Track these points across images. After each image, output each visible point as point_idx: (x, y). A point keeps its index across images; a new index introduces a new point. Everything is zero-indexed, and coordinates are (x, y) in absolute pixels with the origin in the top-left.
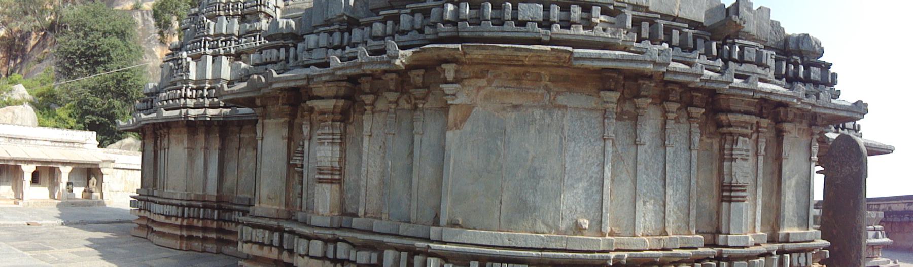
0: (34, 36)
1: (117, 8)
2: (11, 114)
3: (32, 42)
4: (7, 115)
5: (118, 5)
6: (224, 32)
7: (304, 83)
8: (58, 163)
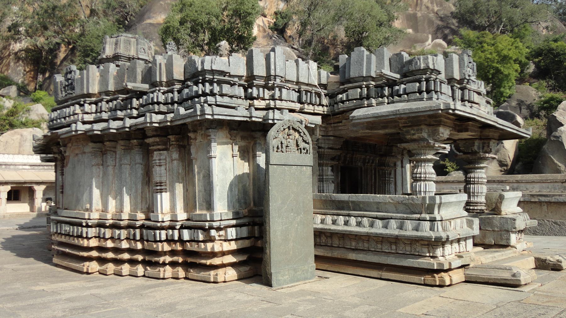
0: (63, 48)
1: (149, 21)
2: (19, 137)
3: (62, 55)
4: (15, 138)
5: (149, 18)
6: (373, 74)
7: (313, 126)
8: (31, 183)
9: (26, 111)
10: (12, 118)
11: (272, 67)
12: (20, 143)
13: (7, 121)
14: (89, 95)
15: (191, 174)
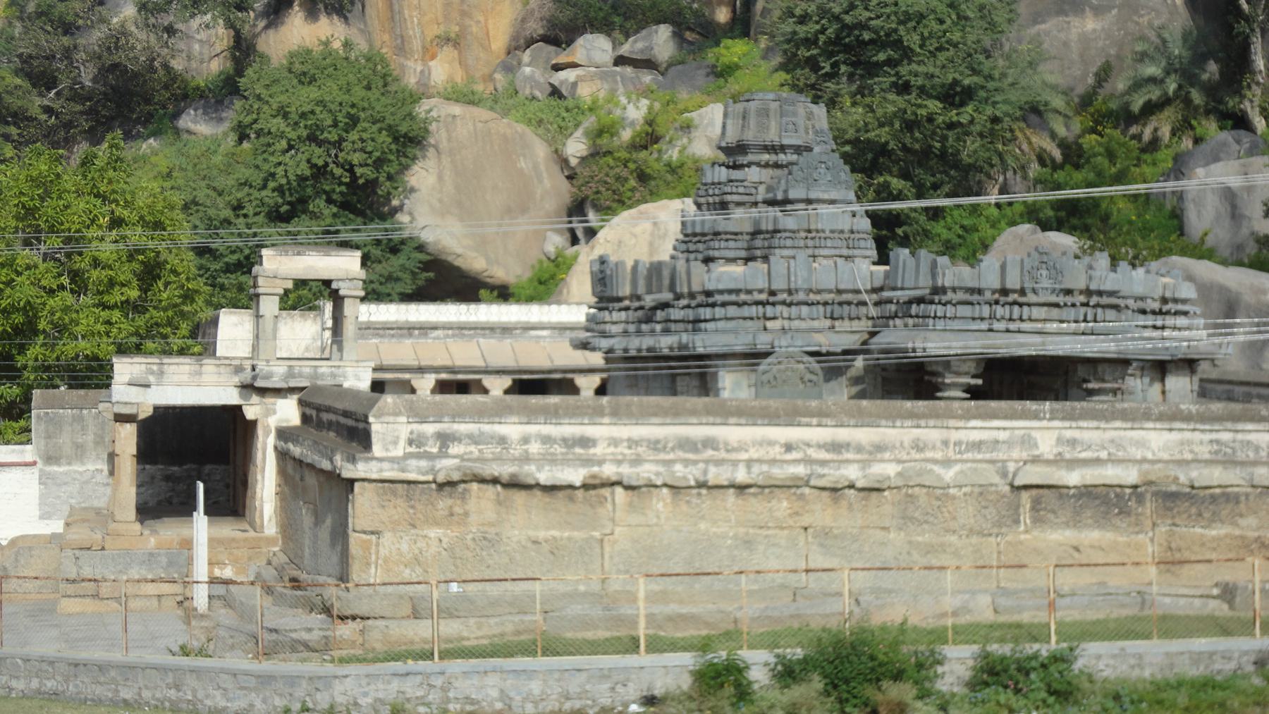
4: (638, 230)
9: (682, 128)
10: (643, 154)
11: (793, 279)
12: (651, 244)
13: (632, 166)
14: (620, 300)
15: (934, 368)
